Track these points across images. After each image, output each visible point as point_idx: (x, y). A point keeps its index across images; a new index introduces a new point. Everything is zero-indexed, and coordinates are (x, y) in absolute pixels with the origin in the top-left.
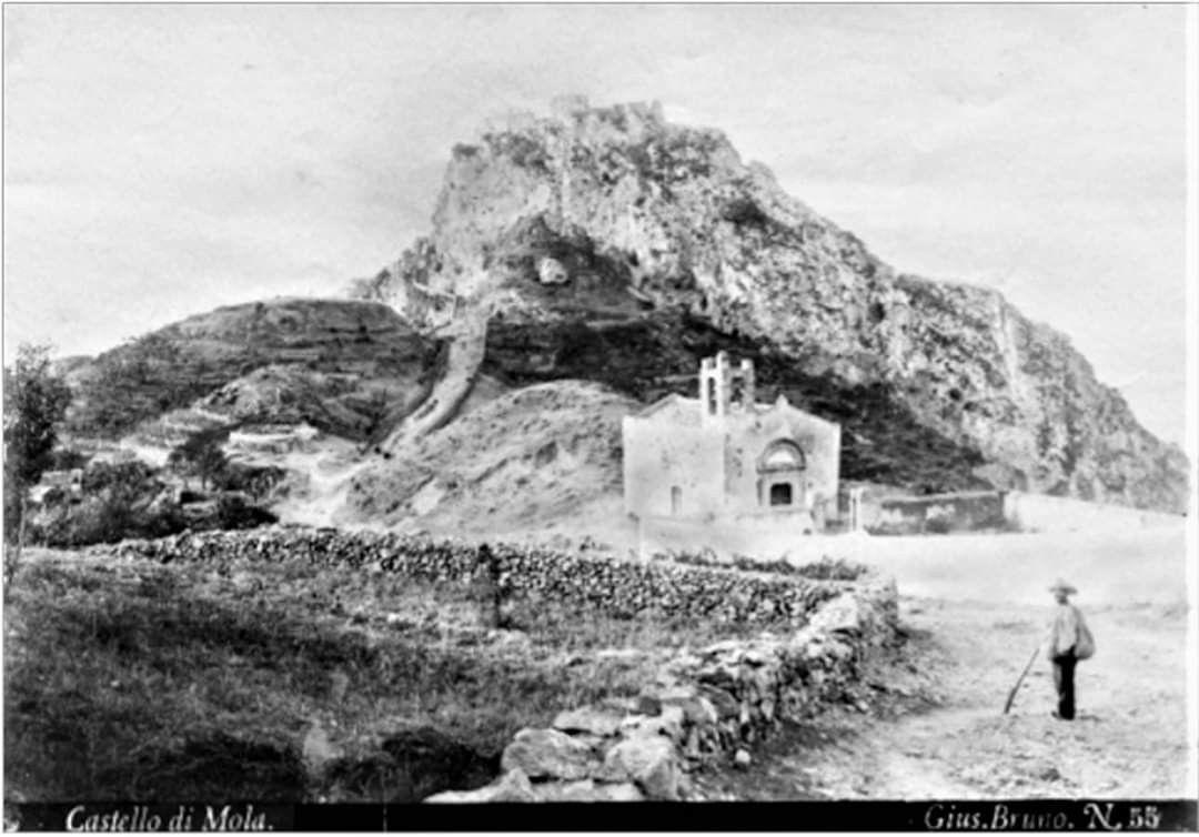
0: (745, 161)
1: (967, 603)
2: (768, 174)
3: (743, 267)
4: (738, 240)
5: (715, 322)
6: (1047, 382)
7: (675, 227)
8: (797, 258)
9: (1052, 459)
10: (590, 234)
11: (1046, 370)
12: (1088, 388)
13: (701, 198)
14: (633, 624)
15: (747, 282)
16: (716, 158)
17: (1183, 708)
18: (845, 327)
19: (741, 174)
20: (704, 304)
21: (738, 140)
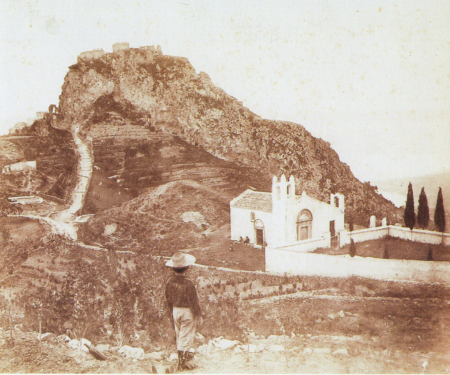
0: (198, 72)
1: (202, 166)
2: (207, 77)
3: (199, 117)
4: (196, 106)
5: (188, 140)
6: (322, 163)
7: (41, 232)
8: (221, 112)
9: (325, 193)
10: (132, 103)
11: (323, 158)
12: (261, 144)
13: (180, 87)
14: (158, 363)
15: (200, 123)
16: (186, 71)
17: (305, 239)
18: (242, 141)
19: (196, 77)
20: (183, 132)
21: (193, 62)
